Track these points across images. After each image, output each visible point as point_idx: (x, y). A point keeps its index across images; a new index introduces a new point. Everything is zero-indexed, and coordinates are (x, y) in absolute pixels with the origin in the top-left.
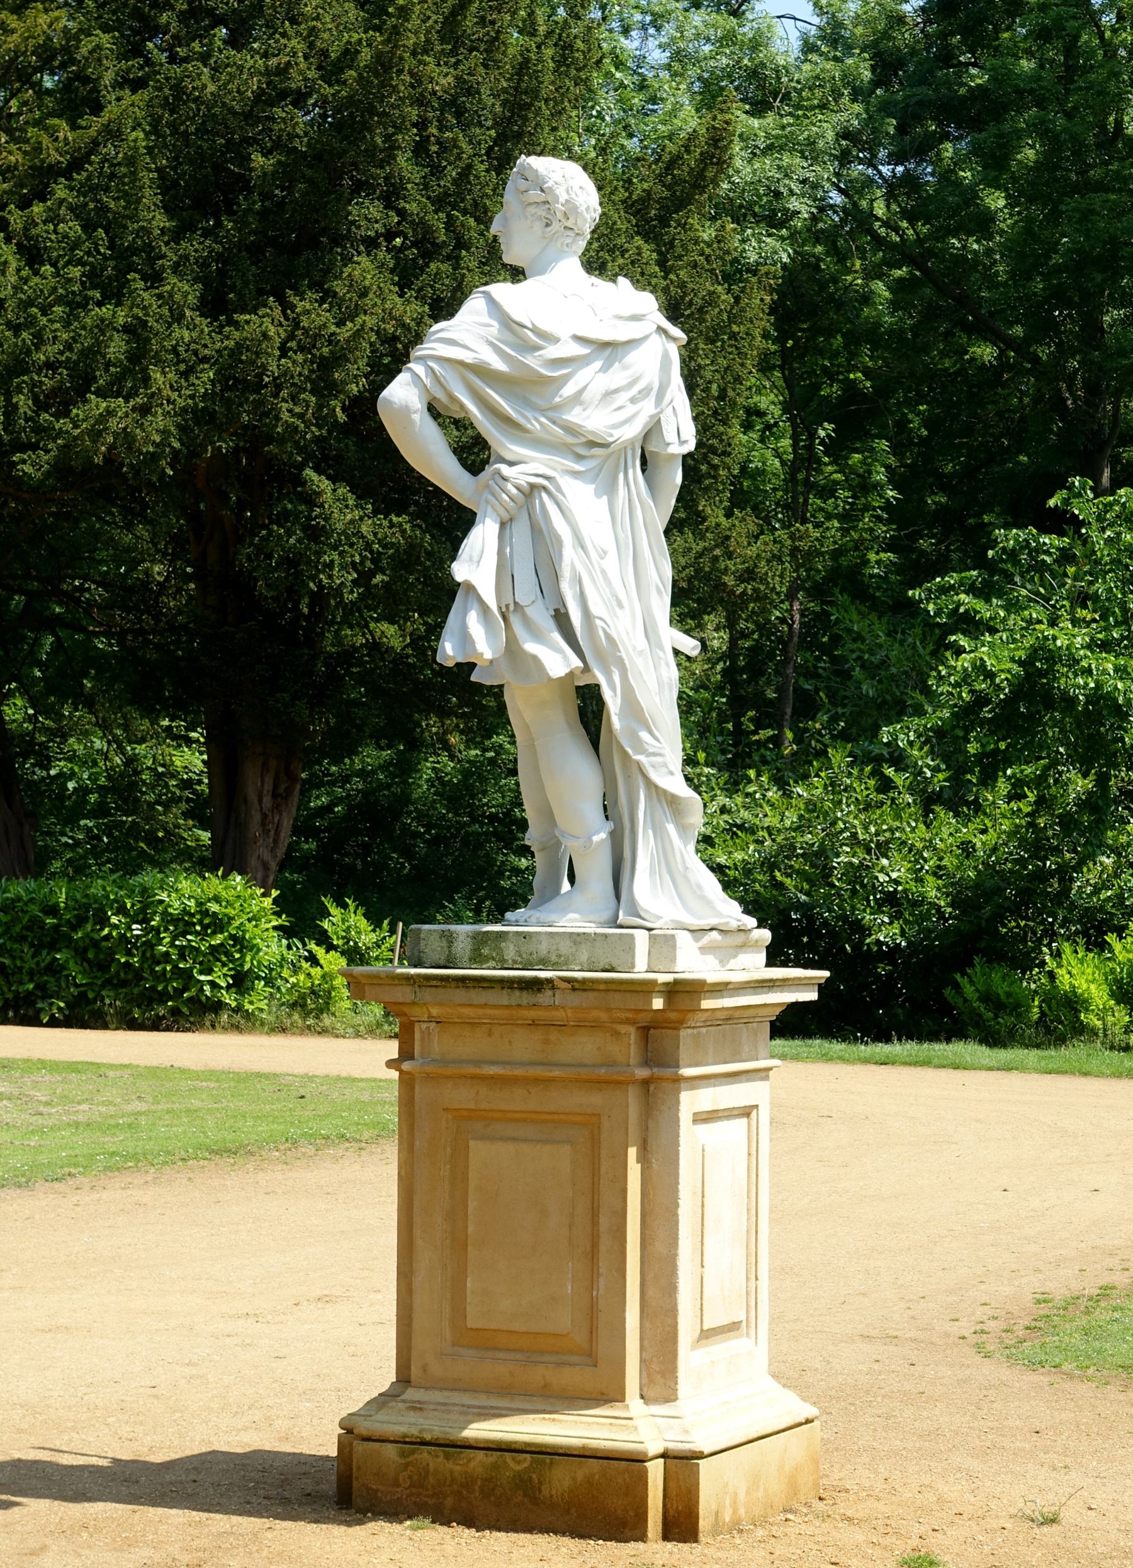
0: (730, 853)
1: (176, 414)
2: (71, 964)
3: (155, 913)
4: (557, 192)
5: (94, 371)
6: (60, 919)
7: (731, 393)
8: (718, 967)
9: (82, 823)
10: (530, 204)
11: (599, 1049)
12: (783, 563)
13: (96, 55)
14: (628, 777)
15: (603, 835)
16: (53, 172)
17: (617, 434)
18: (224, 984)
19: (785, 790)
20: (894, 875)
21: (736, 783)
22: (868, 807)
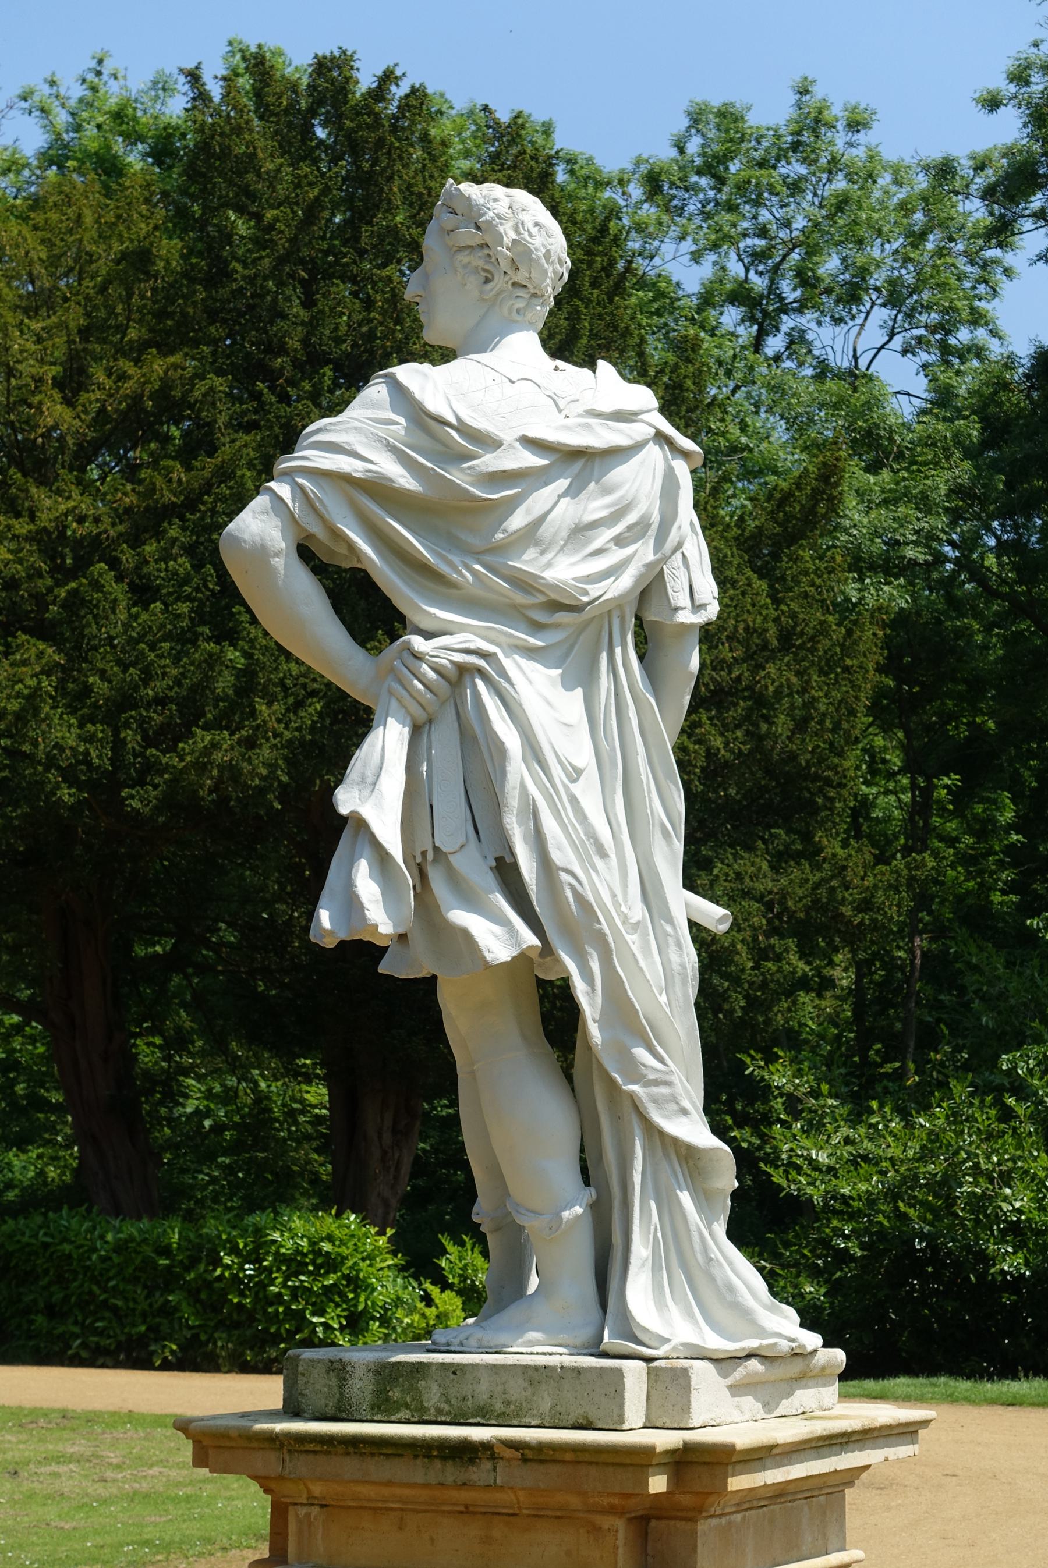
0: (855, 1184)
1: (283, 747)
2: (184, 1305)
3: (268, 1253)
4: (501, 229)
5: (204, 706)
6: (173, 1260)
7: (845, 725)
8: (761, 1414)
9: (220, 1160)
10: (461, 249)
11: (568, 1553)
12: (900, 892)
13: (209, 398)
14: (617, 1118)
15: (578, 1210)
16: (169, 512)
17: (595, 590)
18: (336, 1326)
19: (907, 1121)
20: (1017, 1205)
21: (859, 1115)
22: (990, 1136)
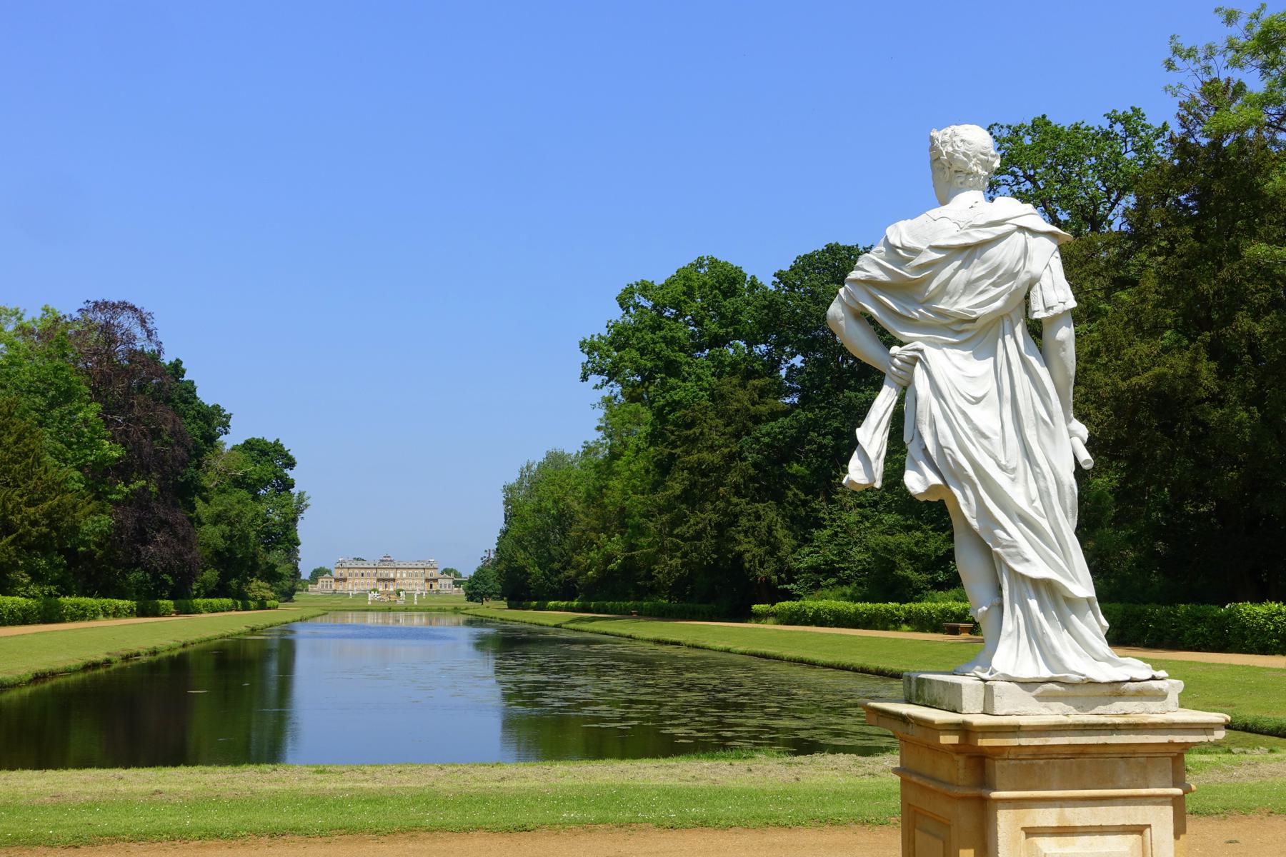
17: (980, 311)
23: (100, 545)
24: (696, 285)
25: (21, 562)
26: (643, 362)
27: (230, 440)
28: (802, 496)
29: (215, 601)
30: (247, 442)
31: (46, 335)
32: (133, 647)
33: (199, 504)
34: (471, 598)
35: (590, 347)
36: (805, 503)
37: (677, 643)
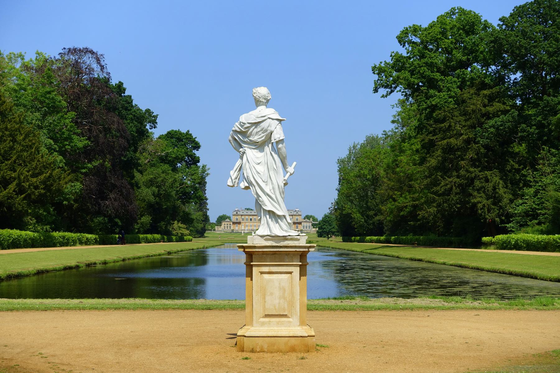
23: (75, 201)
24: (448, 27)
25: (30, 211)
26: (412, 80)
27: (158, 132)
28: (516, 166)
29: (149, 236)
30: (169, 133)
31: (40, 70)
32: (92, 259)
33: (137, 175)
34: (320, 235)
35: (379, 70)
36: (518, 171)
37: (420, 260)
